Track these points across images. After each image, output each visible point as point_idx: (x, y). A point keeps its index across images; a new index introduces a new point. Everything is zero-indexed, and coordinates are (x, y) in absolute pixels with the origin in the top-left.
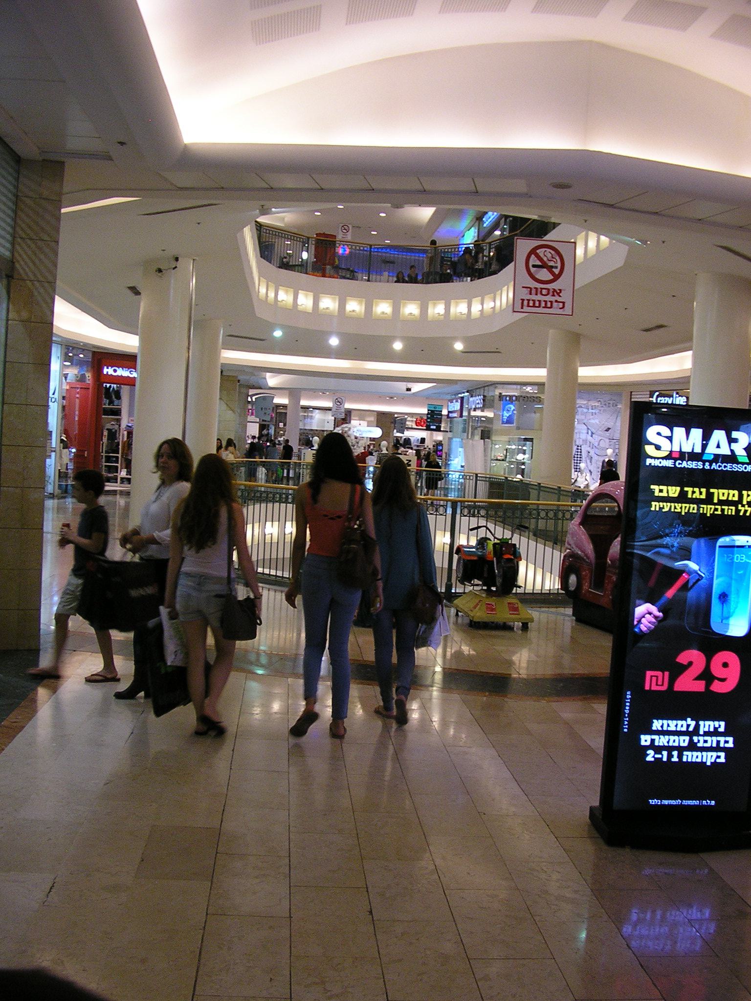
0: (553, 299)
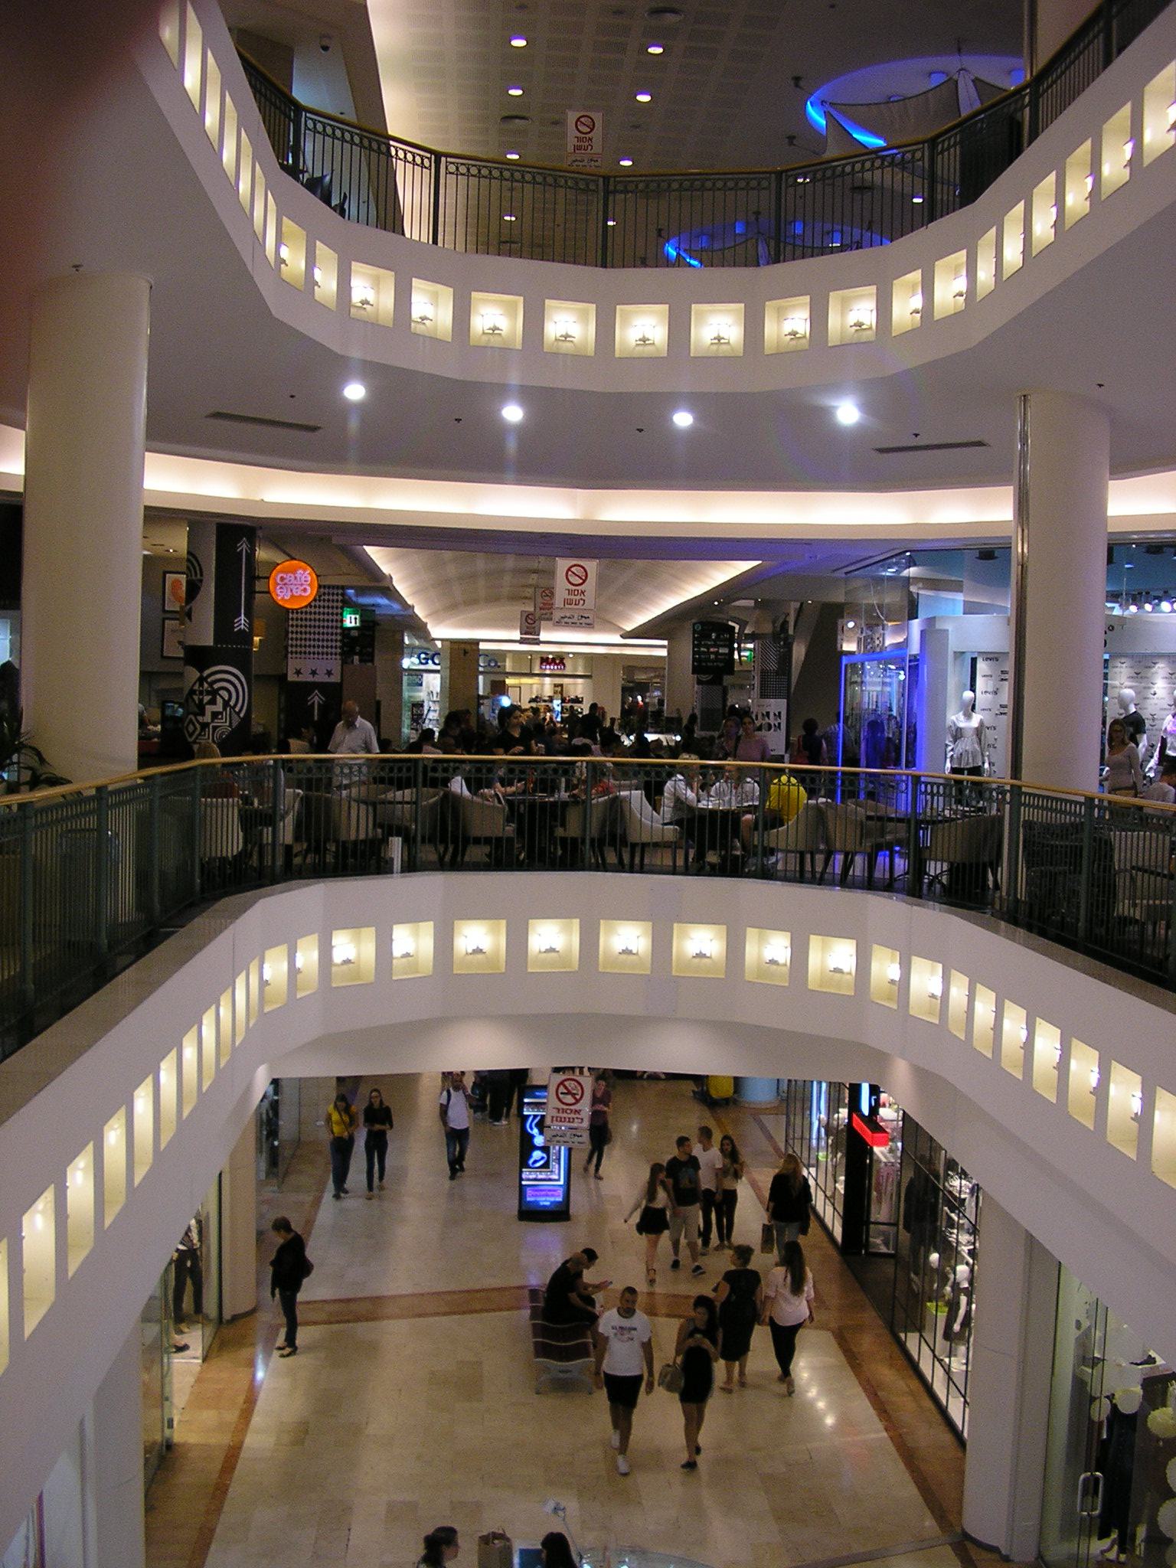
0: (574, 1116)
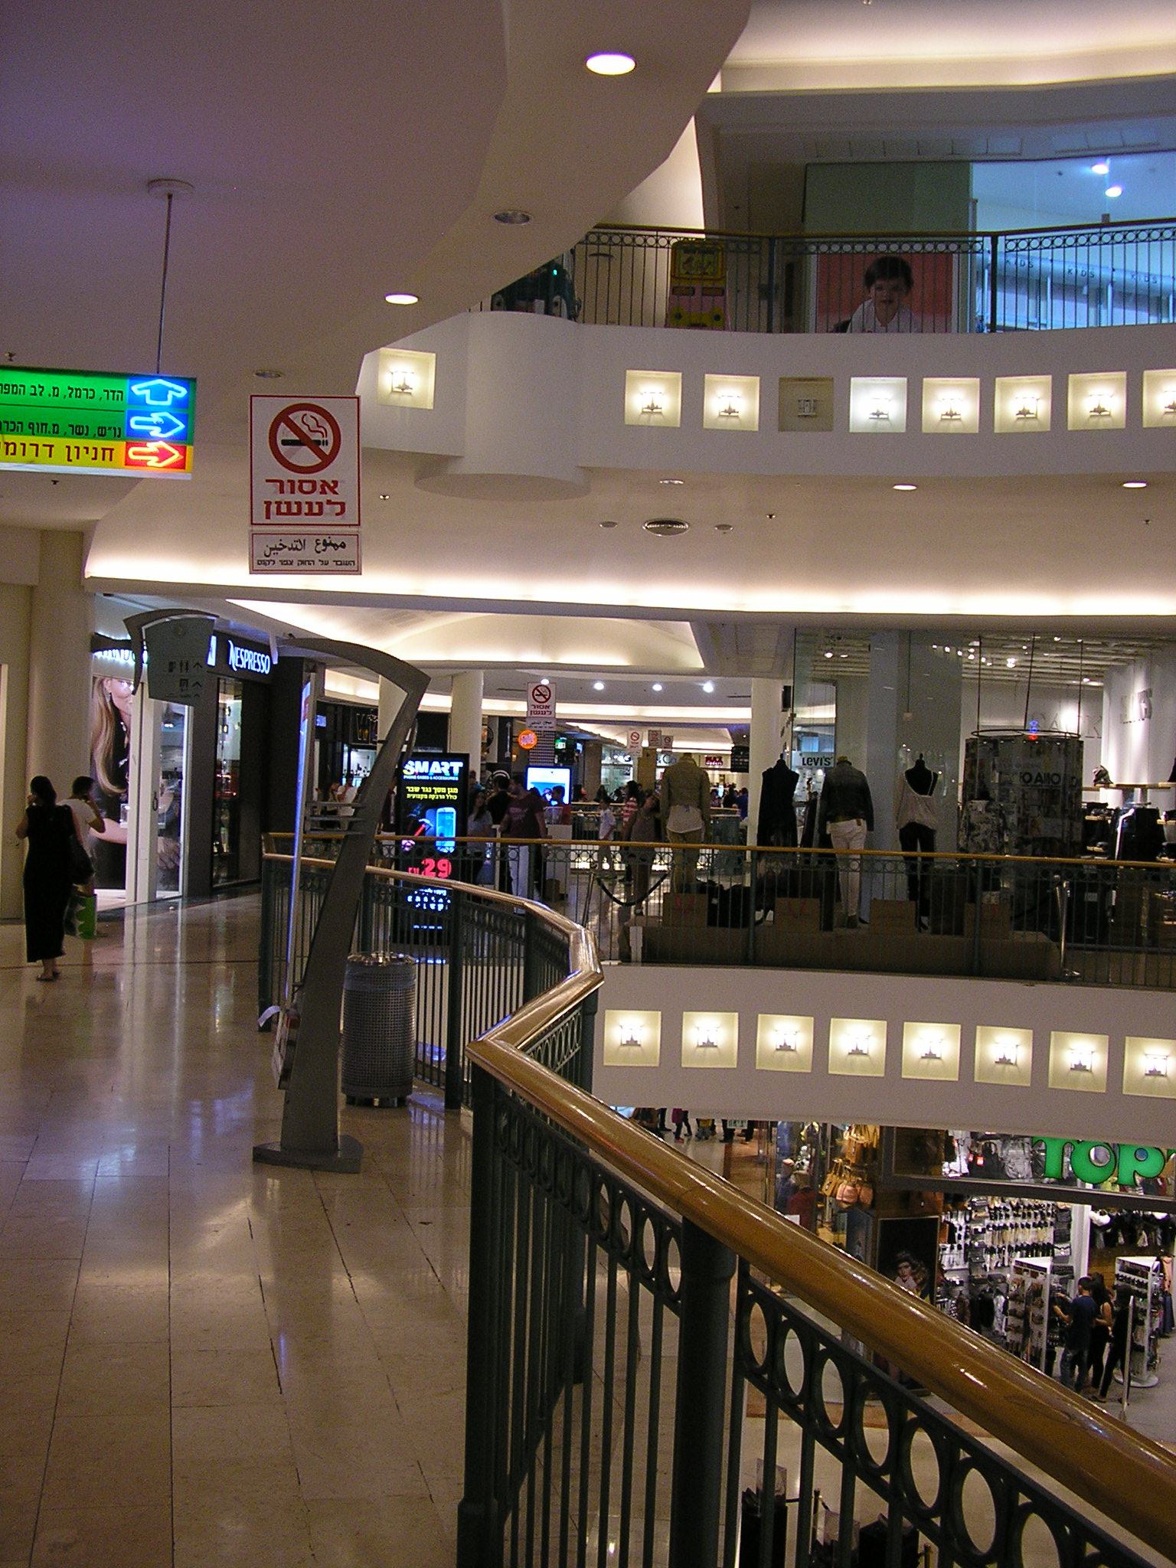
0: (323, 498)
